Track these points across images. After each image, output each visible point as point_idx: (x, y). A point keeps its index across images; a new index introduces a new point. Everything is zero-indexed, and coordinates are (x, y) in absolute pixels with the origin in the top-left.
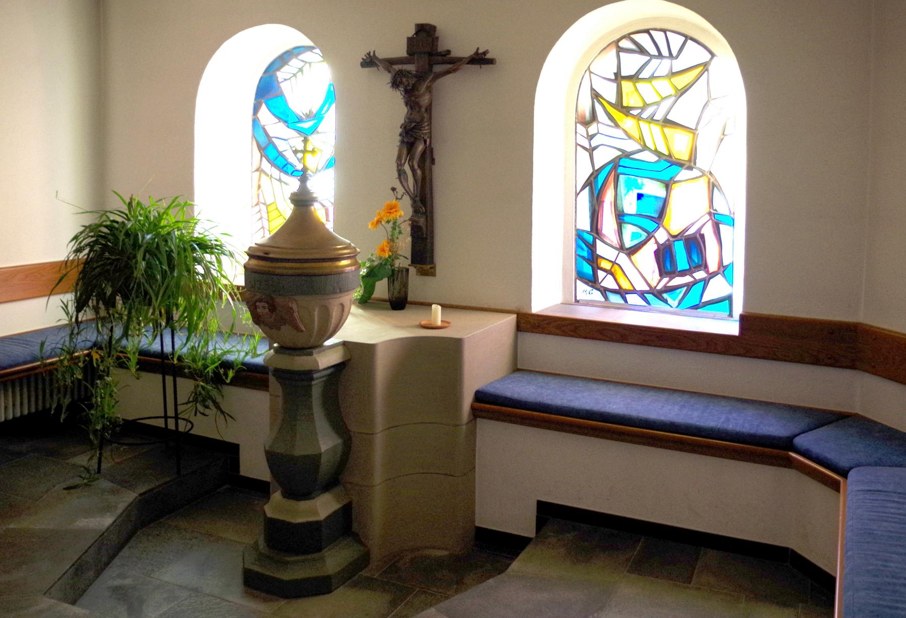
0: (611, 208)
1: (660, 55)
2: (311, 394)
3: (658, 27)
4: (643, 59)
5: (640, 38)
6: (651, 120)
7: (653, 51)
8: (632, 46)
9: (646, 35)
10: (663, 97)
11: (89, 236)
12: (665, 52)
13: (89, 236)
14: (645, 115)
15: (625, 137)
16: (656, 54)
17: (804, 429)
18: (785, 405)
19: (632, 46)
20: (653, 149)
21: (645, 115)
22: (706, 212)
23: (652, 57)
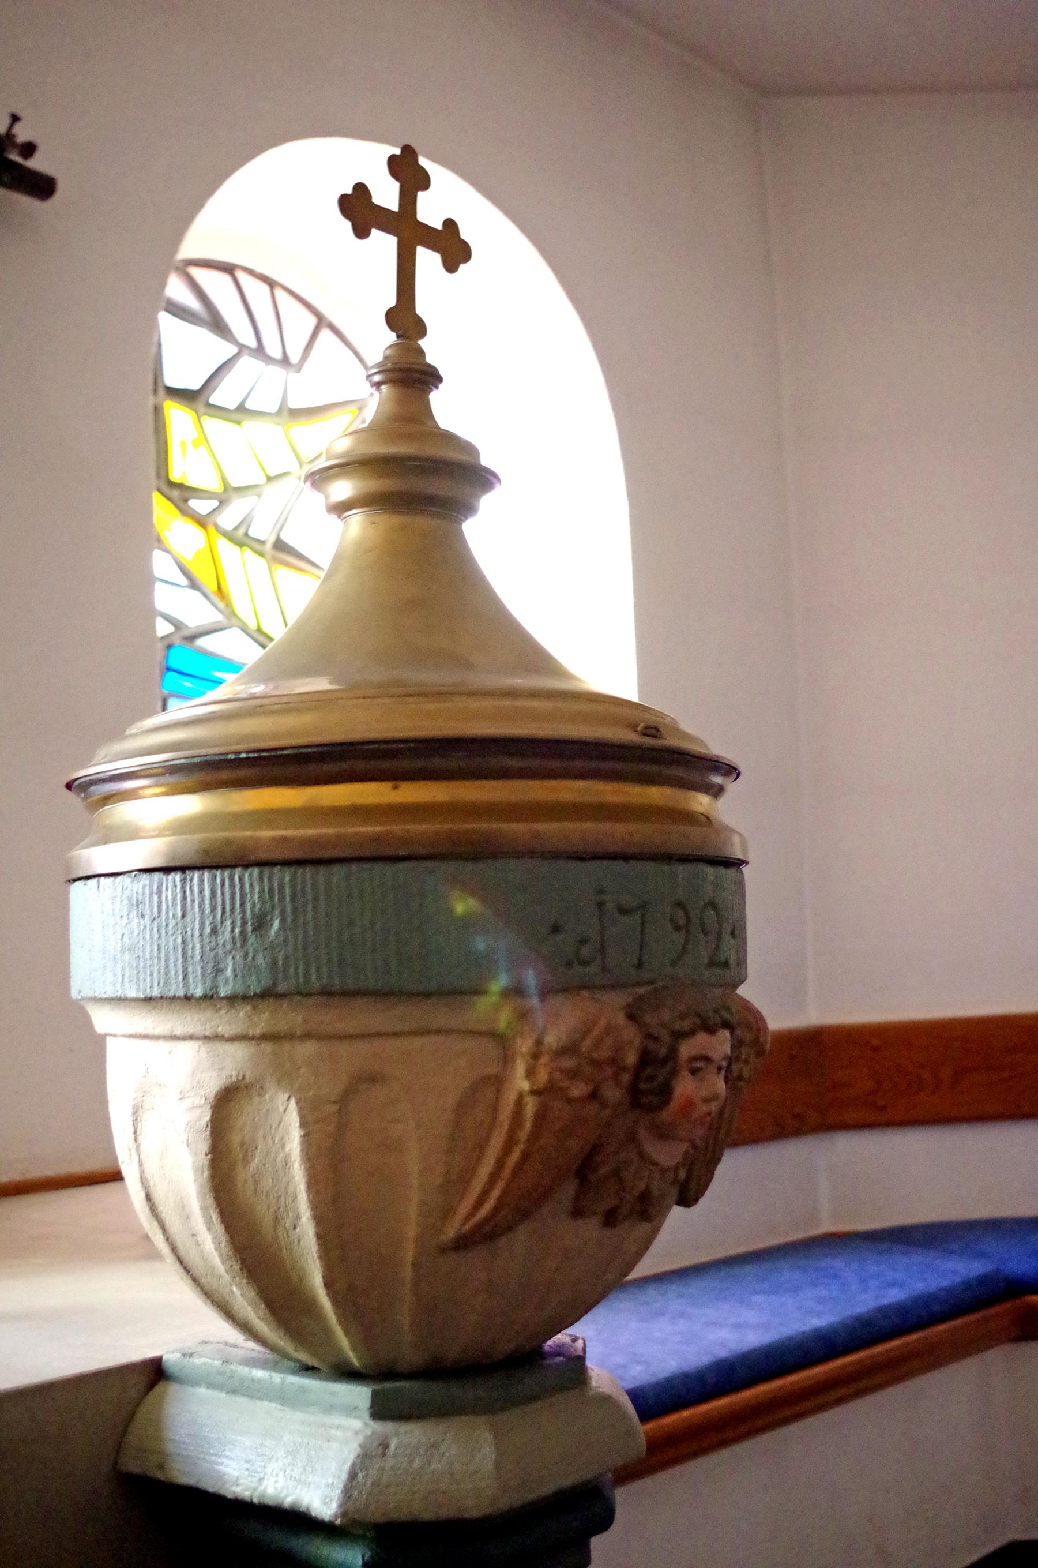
0: (145, 764)
1: (260, 351)
2: (479, 1209)
3: (259, 269)
4: (222, 350)
5: (213, 283)
6: (240, 539)
7: (244, 334)
8: (191, 302)
9: (225, 278)
10: (272, 474)
11: (257, 1173)
12: (273, 349)
13: (257, 1173)
14: (228, 519)
15: (185, 582)
16: (253, 343)
17: (924, 1130)
18: (146, 798)
19: (191, 302)
20: (252, 626)
21: (228, 519)
22: (588, 1355)
23: (242, 348)
